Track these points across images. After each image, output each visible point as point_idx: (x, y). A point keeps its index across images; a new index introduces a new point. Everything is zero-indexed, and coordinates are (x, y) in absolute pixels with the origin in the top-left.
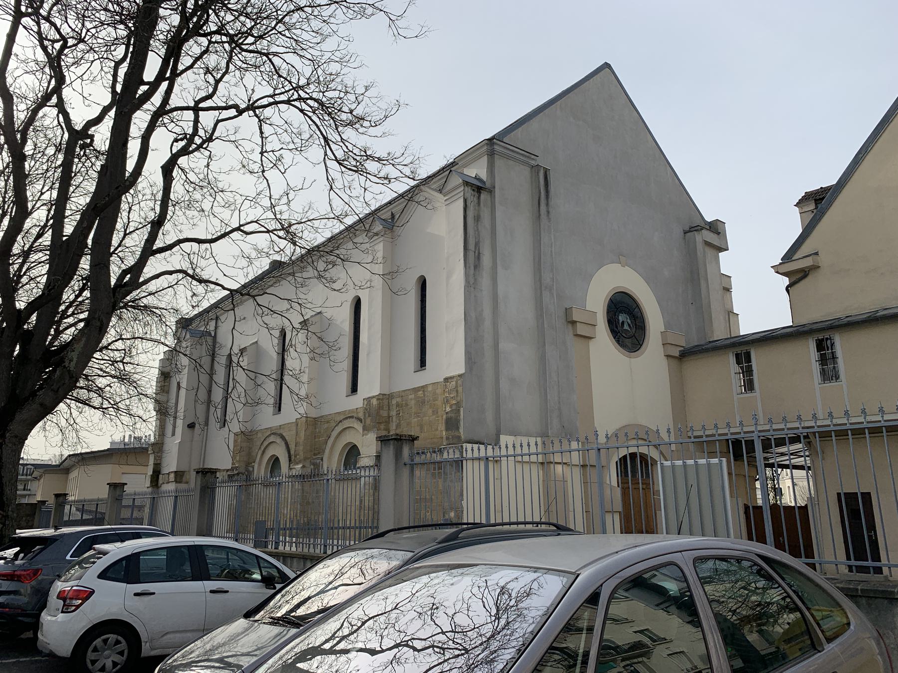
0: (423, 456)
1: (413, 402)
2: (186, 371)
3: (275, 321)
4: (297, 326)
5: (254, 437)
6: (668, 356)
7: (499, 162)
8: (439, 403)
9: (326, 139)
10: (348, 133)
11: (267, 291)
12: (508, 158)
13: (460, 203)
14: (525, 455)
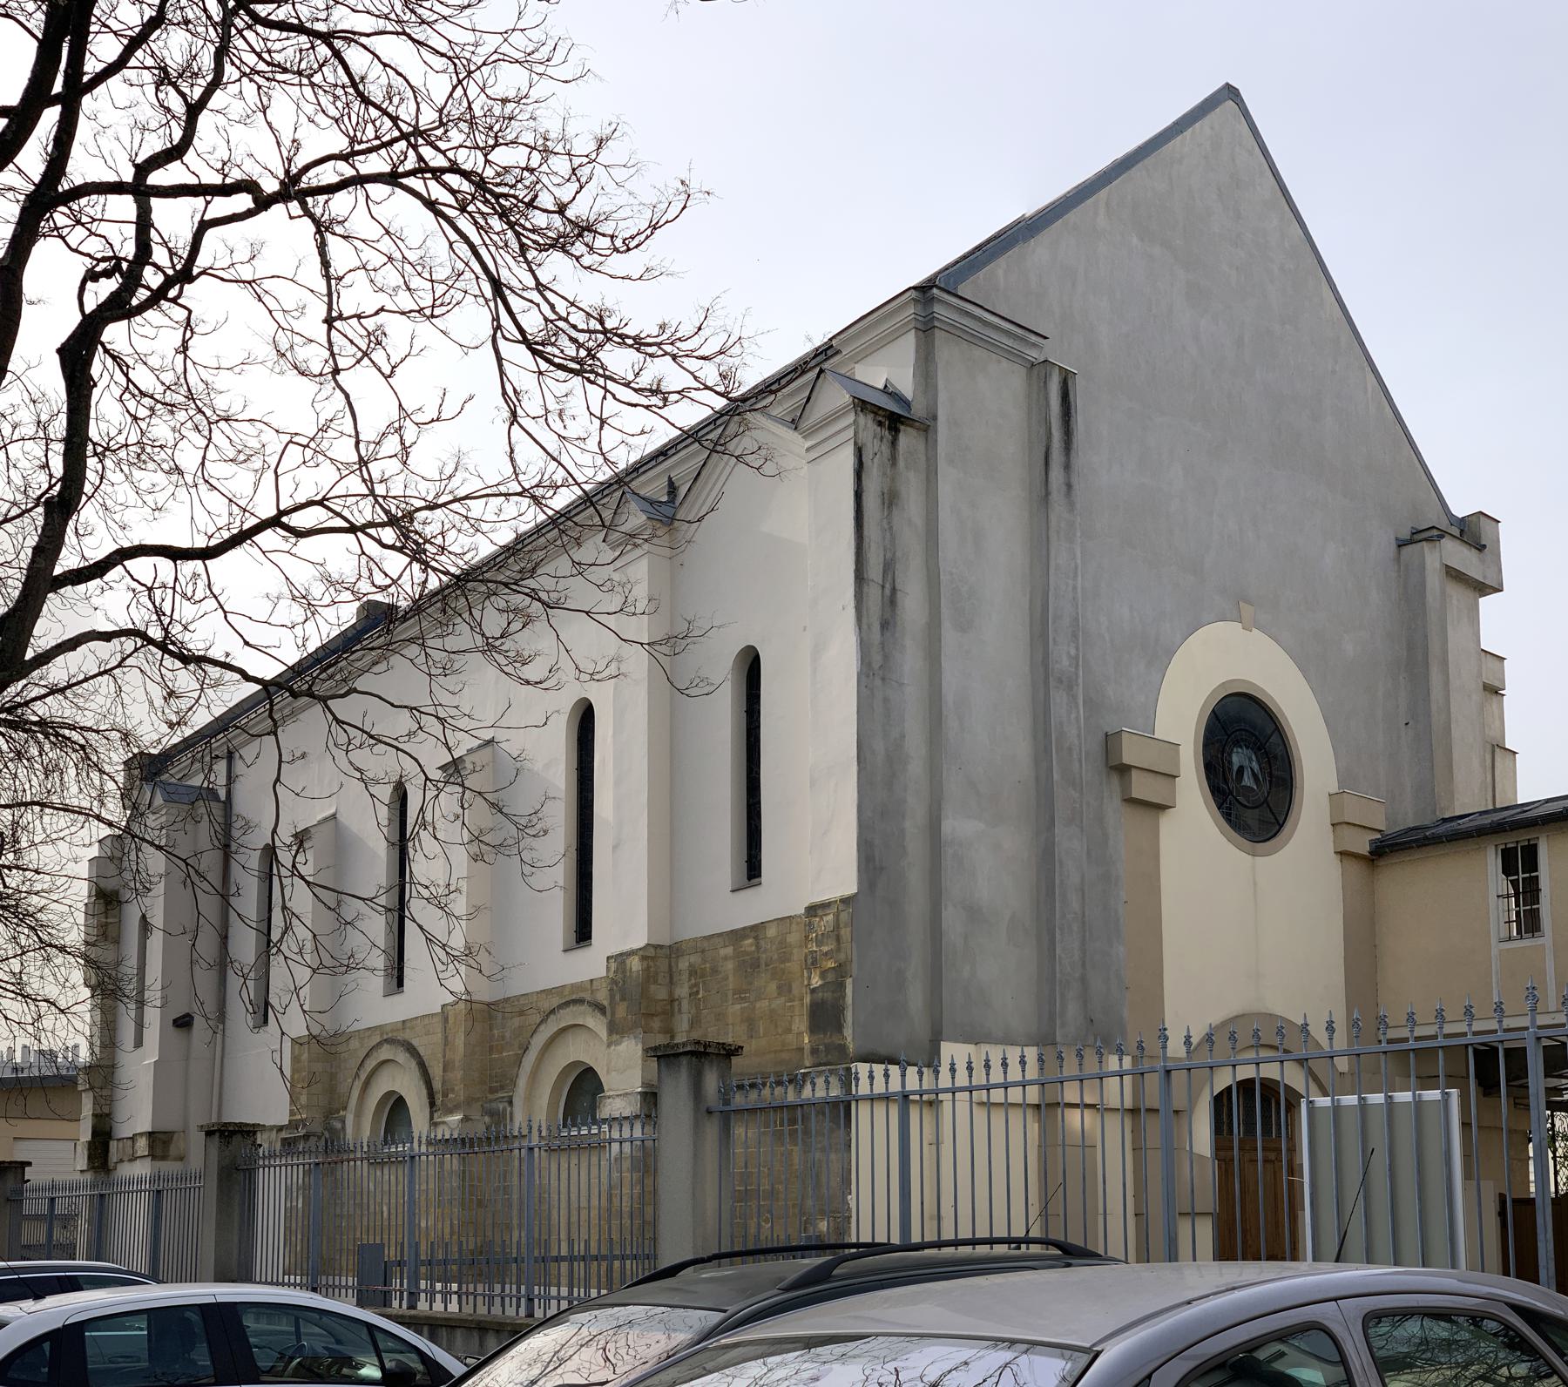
0: (753, 1095)
1: (730, 965)
2: (159, 889)
3: (383, 764)
4: (436, 775)
5: (340, 1048)
6: (1343, 854)
7: (947, 352)
8: (794, 966)
9: (497, 285)
10: (554, 266)
11: (360, 684)
12: (973, 339)
13: (847, 457)
14: (996, 1086)
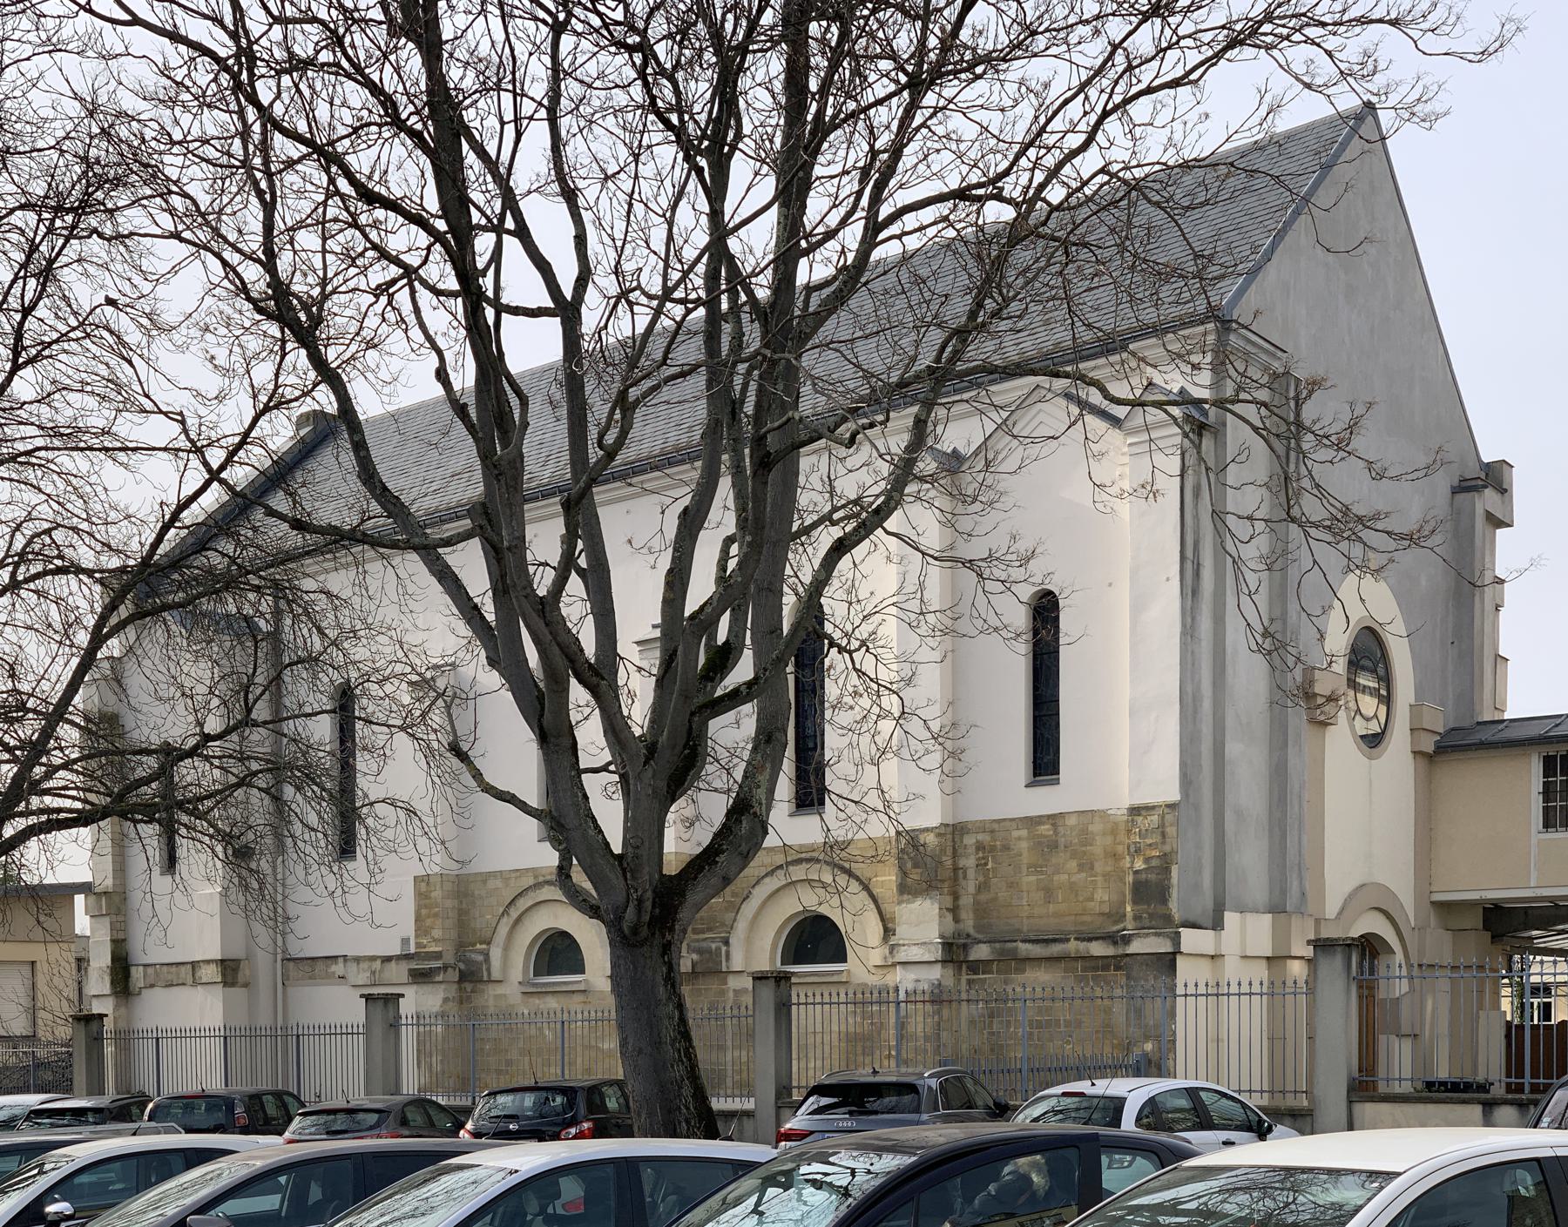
1: (1024, 845)
